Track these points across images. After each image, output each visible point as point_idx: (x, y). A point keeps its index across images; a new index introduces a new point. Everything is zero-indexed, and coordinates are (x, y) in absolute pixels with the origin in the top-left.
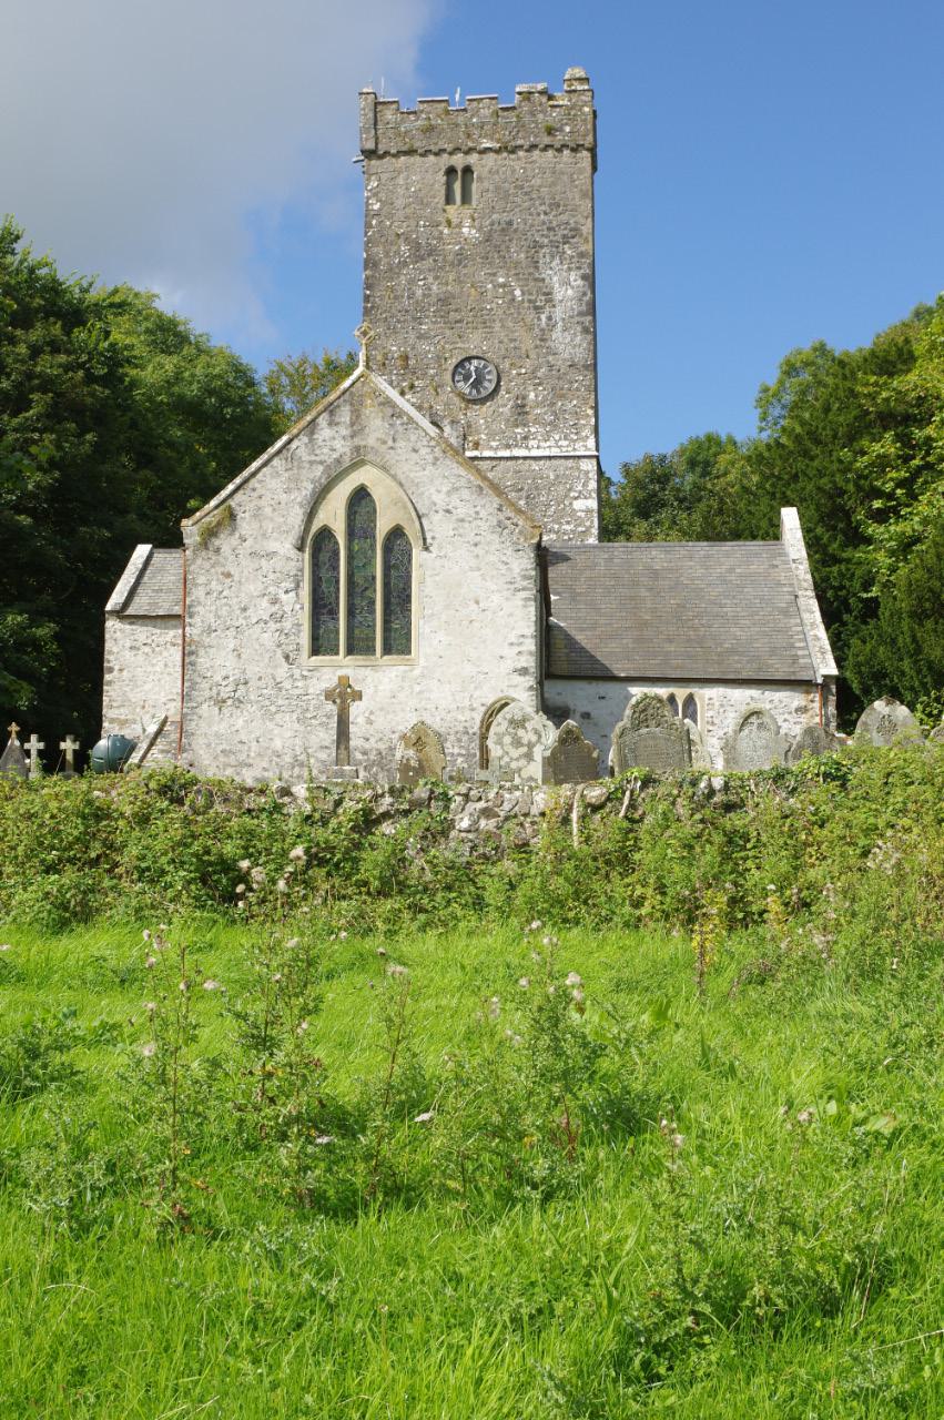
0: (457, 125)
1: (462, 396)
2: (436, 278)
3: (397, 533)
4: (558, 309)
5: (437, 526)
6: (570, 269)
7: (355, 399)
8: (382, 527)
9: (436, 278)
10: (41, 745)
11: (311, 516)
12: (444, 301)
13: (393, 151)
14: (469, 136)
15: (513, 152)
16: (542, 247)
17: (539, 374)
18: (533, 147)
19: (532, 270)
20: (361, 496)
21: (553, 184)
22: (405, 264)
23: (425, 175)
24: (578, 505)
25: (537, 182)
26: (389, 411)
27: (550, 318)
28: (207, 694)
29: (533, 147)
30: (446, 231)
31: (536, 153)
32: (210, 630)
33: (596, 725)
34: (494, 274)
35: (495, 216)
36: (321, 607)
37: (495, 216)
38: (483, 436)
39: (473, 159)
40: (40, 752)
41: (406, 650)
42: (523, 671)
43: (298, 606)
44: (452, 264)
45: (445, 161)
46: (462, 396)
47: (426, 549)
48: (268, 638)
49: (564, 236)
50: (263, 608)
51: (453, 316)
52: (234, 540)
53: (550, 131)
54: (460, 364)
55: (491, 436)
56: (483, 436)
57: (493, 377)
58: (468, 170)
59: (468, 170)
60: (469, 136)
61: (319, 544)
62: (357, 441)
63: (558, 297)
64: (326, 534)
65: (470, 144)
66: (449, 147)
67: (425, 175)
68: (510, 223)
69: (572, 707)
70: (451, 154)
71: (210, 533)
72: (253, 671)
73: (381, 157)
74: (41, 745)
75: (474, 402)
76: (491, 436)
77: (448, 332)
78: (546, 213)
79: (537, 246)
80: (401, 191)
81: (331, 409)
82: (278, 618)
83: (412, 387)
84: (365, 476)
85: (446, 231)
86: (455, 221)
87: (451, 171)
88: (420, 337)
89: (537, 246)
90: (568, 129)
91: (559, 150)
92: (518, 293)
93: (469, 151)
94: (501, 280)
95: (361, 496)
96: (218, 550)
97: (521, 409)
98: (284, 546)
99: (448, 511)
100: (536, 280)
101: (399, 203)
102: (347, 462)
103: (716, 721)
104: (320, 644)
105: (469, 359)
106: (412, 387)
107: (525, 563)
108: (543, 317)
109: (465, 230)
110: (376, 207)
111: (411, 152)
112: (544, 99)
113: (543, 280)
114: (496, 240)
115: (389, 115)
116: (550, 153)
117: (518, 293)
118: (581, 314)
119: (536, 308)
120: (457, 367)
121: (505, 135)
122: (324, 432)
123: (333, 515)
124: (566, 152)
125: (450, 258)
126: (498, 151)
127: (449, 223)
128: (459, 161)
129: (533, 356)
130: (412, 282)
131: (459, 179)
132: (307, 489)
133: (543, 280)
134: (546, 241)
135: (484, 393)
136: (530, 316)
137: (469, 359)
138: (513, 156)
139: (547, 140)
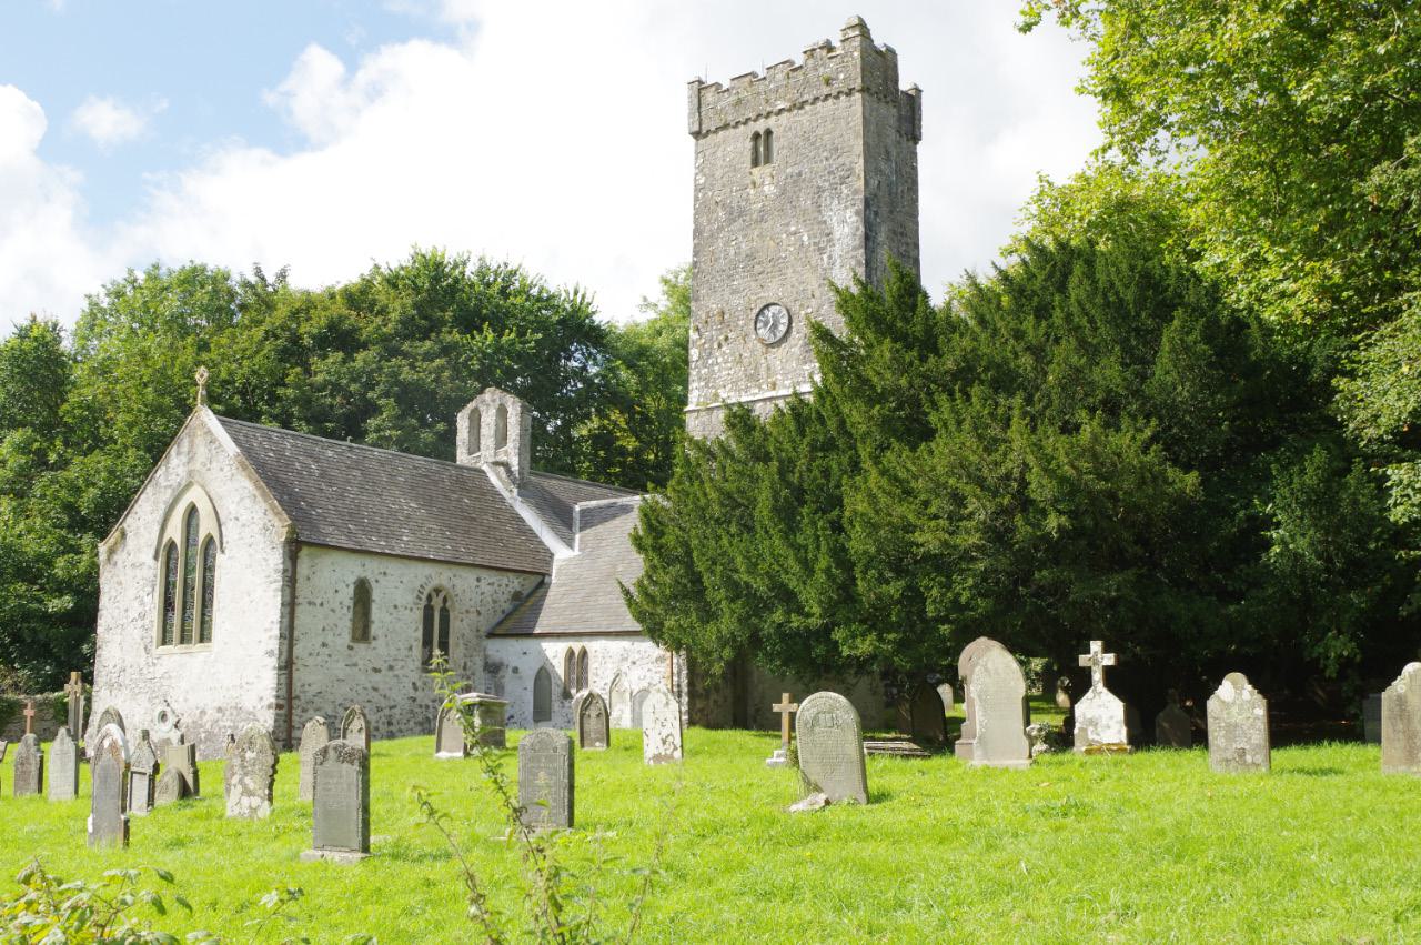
0: (759, 94)
1: (762, 341)
2: (745, 236)
3: (210, 540)
4: (837, 247)
6: (846, 207)
8: (202, 537)
9: (745, 236)
10: (1109, 660)
12: (751, 257)
13: (713, 129)
14: (767, 101)
15: (801, 108)
16: (823, 191)
17: (822, 312)
18: (816, 99)
19: (816, 214)
21: (834, 130)
22: (721, 228)
23: (737, 144)
25: (819, 132)
26: (209, 438)
27: (830, 257)
28: (104, 679)
29: (816, 99)
30: (752, 192)
31: (820, 104)
33: (520, 678)
34: (788, 224)
35: (789, 170)
37: (789, 170)
38: (779, 377)
39: (772, 122)
40: (1107, 671)
41: (210, 640)
42: (270, 653)
43: (153, 603)
44: (756, 221)
46: (762, 341)
47: (223, 552)
48: (137, 633)
49: (841, 178)
51: (758, 268)
52: (124, 555)
53: (828, 82)
54: (761, 312)
56: (779, 377)
57: (785, 320)
58: (769, 133)
59: (769, 133)
60: (767, 101)
62: (191, 467)
63: (837, 235)
64: (172, 545)
65: (769, 109)
66: (752, 115)
68: (800, 174)
69: (506, 663)
70: (755, 121)
71: (112, 551)
73: (705, 136)
74: (1109, 660)
75: (772, 345)
77: (753, 284)
78: (827, 159)
79: (820, 190)
80: (720, 163)
82: (142, 616)
83: (727, 339)
84: (195, 495)
85: (752, 192)
86: (758, 182)
88: (734, 292)
89: (820, 190)
90: (842, 76)
91: (837, 97)
92: (805, 238)
93: (768, 115)
94: (793, 228)
95: (192, 511)
96: (115, 564)
98: (147, 556)
99: (237, 519)
100: (819, 223)
101: (718, 174)
102: (184, 483)
103: (600, 672)
105: (767, 306)
106: (727, 339)
107: (276, 559)
108: (825, 257)
109: (766, 188)
110: (702, 181)
111: (726, 127)
112: (824, 52)
113: (825, 222)
115: (709, 97)
116: (830, 101)
117: (805, 238)
118: (855, 249)
119: (819, 249)
120: (758, 316)
121: (793, 95)
123: (175, 532)
124: (843, 97)
125: (754, 216)
126: (789, 110)
127: (754, 184)
128: (761, 126)
129: (817, 294)
130: (727, 243)
132: (162, 508)
133: (825, 222)
134: (827, 184)
135: (779, 335)
136: (814, 257)
137: (767, 306)
138: (801, 112)
139: (826, 90)
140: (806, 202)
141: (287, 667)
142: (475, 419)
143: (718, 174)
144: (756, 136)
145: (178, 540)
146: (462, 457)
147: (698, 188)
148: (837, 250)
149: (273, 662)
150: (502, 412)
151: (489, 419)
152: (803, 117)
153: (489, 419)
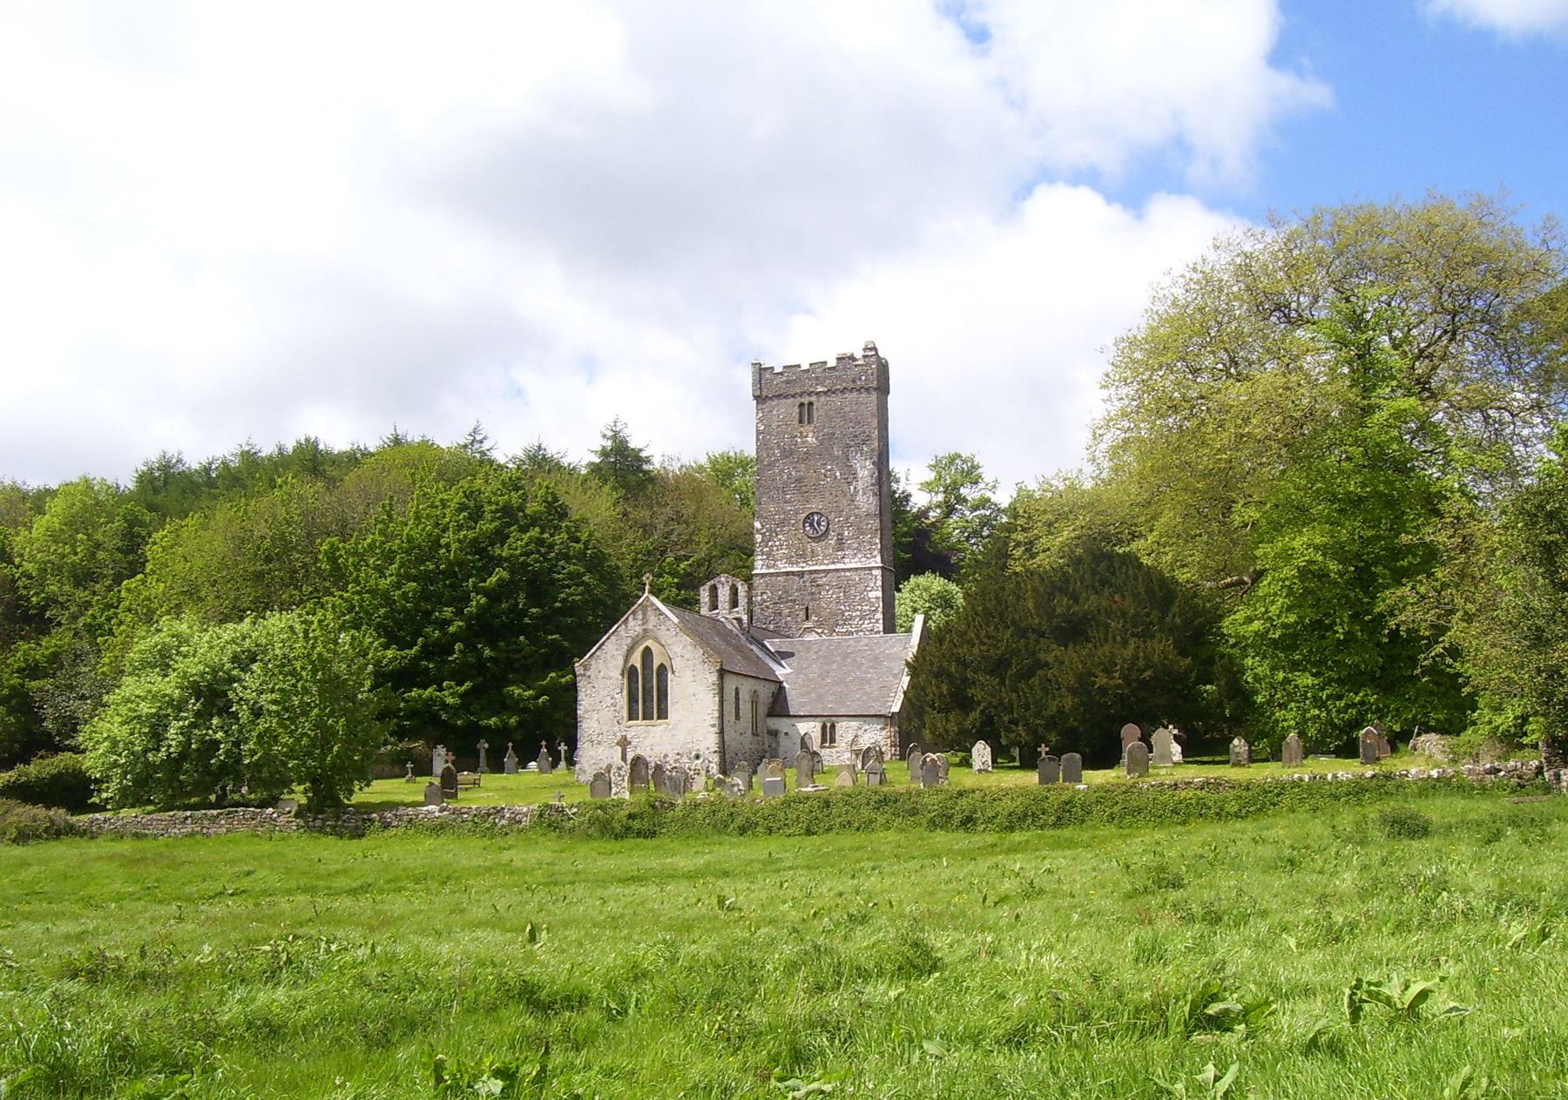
3: (662, 666)
5: (677, 663)
7: (644, 608)
11: (626, 661)
12: (799, 480)
20: (647, 653)
23: (788, 409)
24: (871, 595)
32: (587, 711)
36: (632, 699)
39: (813, 399)
43: (622, 700)
45: (799, 400)
48: (610, 715)
50: (609, 701)
55: (825, 557)
59: (811, 404)
61: (631, 673)
64: (633, 670)
67: (788, 409)
72: (605, 728)
76: (825, 557)
81: (634, 613)
87: (802, 405)
97: (840, 541)
98: (616, 674)
101: (774, 425)
104: (632, 716)
107: (714, 678)
114: (827, 440)
122: (631, 623)
123: (636, 660)
128: (806, 400)
131: (806, 413)
136: (845, 487)
140: (837, 452)
141: (721, 732)
142: (714, 589)
143: (774, 425)
144: (802, 405)
145: (638, 665)
146: (704, 611)
147: (758, 432)
148: (860, 485)
149: (716, 729)
150: (734, 591)
151: (724, 594)
152: (836, 400)
153: (724, 594)
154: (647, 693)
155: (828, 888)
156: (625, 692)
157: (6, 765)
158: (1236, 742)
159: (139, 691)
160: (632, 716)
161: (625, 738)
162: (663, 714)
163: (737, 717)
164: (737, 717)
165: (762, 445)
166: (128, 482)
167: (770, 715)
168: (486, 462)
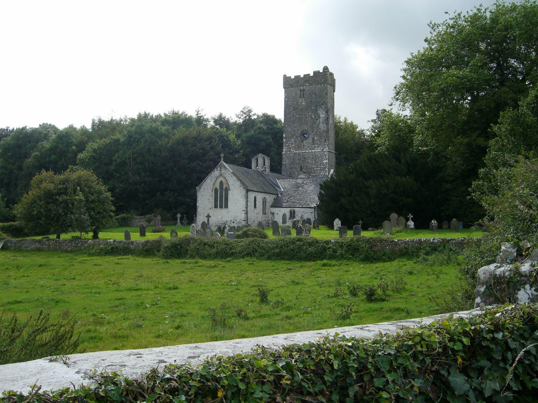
11: (214, 185)
24: (324, 161)
36: (216, 200)
55: (308, 147)
61: (216, 190)
104: (216, 207)
145: (218, 188)
151: (260, 161)
153: (260, 161)
154: (221, 199)
155: (17, 239)
156: (214, 197)
157: (2, 222)
158: (433, 222)
159: (33, 193)
160: (216, 207)
161: (208, 214)
162: (226, 206)
163: (255, 207)
164: (255, 207)
165: (290, 106)
166: (293, 77)
167: (273, 206)
168: (75, 129)
